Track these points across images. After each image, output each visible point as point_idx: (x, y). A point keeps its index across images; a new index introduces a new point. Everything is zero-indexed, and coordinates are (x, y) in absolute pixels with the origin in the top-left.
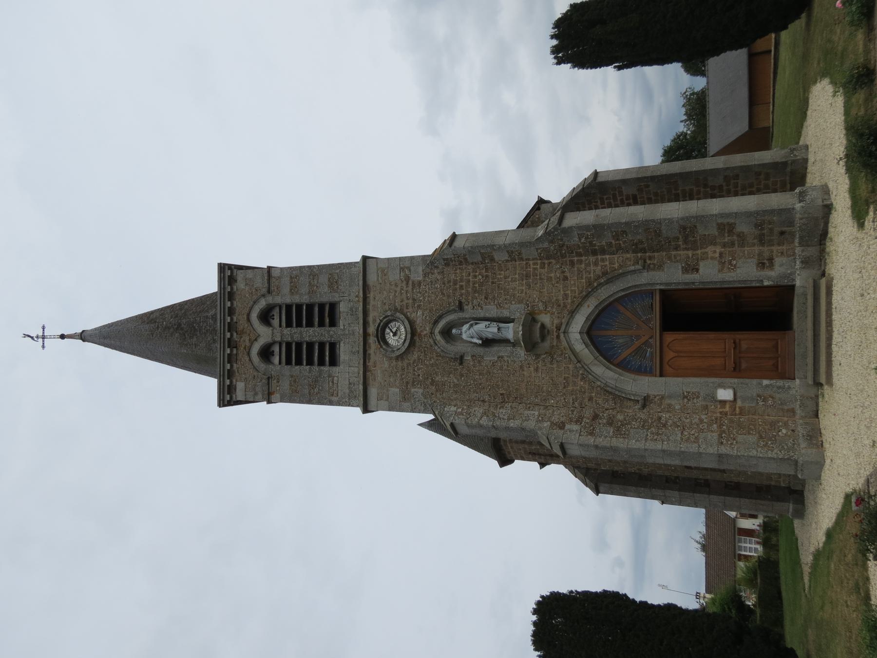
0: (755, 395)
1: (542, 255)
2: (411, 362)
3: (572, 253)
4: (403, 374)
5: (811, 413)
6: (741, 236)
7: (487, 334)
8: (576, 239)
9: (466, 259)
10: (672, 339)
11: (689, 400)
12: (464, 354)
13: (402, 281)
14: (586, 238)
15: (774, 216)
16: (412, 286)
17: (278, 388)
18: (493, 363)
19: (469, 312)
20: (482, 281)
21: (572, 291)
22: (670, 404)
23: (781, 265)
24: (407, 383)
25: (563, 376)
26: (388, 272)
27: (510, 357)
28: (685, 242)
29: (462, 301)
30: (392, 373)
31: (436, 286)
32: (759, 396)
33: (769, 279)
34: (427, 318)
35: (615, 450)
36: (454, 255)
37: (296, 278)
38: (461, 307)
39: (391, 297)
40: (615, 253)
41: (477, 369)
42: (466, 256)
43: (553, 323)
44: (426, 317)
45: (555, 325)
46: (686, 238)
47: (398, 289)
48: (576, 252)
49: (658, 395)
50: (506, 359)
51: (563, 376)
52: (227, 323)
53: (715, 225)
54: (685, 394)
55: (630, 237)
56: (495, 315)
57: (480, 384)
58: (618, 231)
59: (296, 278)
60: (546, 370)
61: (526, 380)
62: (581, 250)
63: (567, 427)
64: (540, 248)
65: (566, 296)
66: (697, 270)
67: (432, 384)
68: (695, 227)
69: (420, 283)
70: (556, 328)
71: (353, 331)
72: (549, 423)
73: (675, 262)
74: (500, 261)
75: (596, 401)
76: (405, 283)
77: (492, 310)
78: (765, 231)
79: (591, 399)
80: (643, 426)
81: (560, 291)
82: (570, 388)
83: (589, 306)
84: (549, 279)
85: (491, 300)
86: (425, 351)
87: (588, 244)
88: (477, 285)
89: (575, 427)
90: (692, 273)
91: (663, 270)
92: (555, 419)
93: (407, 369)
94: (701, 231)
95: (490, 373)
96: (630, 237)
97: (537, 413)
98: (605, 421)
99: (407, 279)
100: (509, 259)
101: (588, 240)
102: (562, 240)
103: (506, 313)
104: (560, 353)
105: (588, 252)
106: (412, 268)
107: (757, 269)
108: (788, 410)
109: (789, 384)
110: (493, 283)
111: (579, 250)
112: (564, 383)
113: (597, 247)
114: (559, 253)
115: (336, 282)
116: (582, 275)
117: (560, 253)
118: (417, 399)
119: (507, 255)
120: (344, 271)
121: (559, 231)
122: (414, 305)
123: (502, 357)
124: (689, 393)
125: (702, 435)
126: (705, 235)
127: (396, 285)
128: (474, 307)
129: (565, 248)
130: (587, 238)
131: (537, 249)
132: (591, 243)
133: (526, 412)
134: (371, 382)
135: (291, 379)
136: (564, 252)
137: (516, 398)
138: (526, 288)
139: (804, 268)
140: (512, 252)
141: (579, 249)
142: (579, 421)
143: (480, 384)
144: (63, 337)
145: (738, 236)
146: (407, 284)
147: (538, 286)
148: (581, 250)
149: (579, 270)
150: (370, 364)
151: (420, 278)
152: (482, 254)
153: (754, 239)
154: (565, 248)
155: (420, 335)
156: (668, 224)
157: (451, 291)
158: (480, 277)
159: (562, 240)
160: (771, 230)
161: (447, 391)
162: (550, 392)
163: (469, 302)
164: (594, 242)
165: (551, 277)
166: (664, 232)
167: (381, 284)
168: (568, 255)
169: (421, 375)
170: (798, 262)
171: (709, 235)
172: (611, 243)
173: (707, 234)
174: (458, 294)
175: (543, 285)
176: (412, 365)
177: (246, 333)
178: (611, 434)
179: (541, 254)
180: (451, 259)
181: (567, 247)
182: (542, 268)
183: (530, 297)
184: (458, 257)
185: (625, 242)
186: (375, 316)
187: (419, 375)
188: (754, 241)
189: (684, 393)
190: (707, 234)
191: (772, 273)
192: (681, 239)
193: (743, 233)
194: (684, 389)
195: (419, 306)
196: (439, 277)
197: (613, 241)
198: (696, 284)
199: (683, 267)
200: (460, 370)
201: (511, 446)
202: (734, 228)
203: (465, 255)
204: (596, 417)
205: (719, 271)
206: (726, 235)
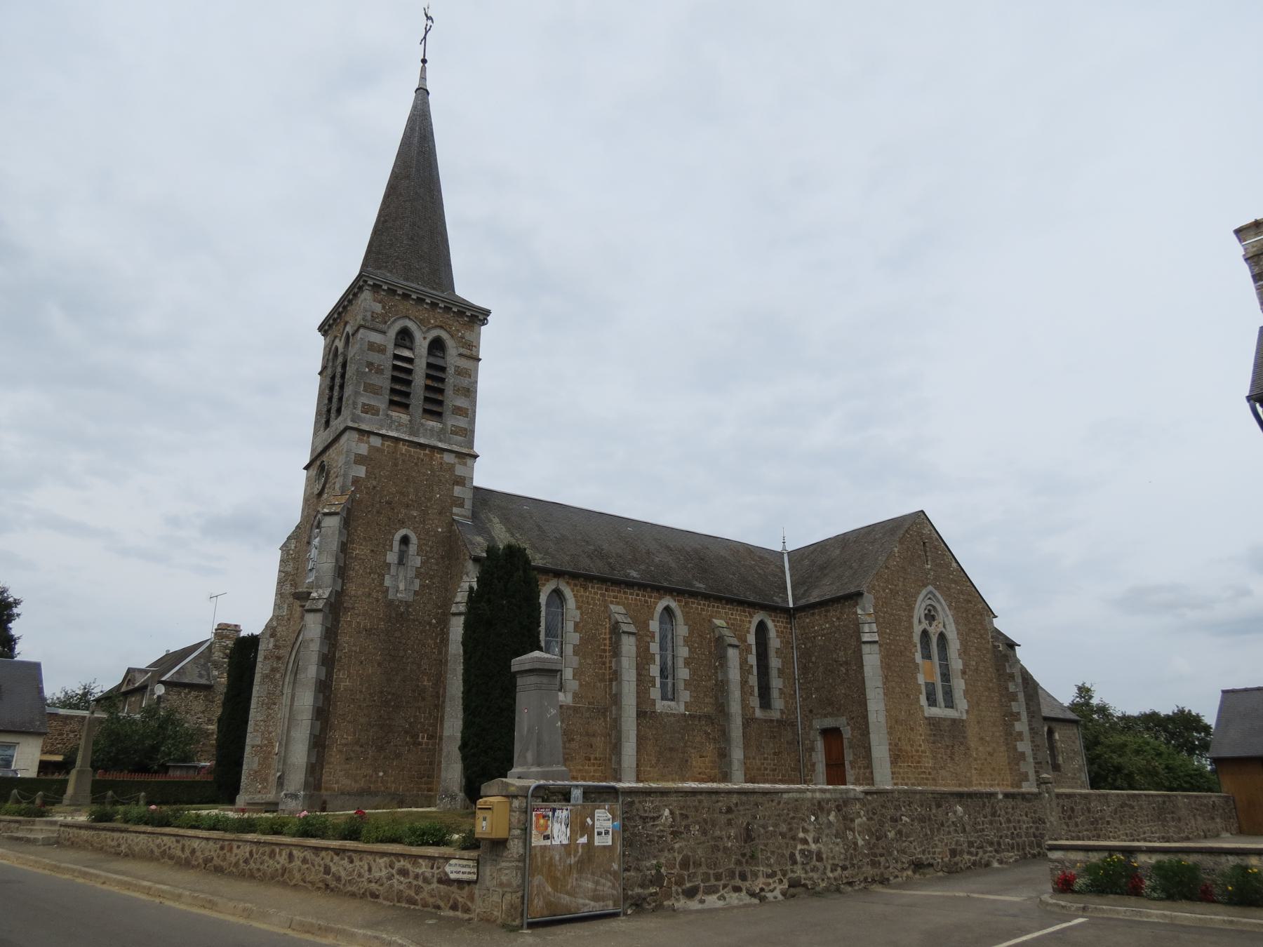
63: (272, 640)
72: (276, 625)
80: (270, 693)
89: (271, 646)
92: (280, 628)
97: (284, 614)
98: (275, 665)
125: (259, 734)
133: (286, 606)
142: (276, 647)
144: (424, 61)
178: (264, 672)
204: (279, 658)
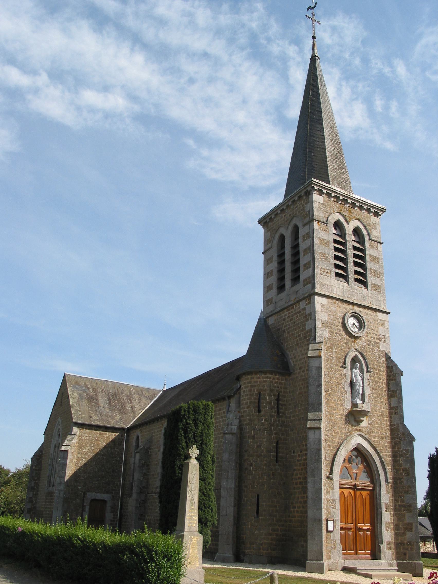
0: (336, 539)
1: (394, 426)
2: (341, 333)
3: (395, 444)
4: (335, 326)
5: (330, 567)
6: (404, 534)
7: (358, 385)
8: (405, 448)
9: (392, 380)
10: (352, 494)
11: (332, 503)
12: (347, 369)
13: (379, 336)
14: (406, 453)
15: (416, 551)
16: (377, 342)
17: (322, 229)
18: (343, 387)
19: (366, 376)
20: (380, 387)
21: (377, 441)
22: (330, 492)
23: (389, 553)
24: (331, 327)
25: (339, 431)
26: (383, 327)
27: (347, 399)
28: (400, 506)
29: (371, 373)
30: (336, 318)
31: (378, 358)
32: (336, 540)
33: (384, 547)
34: (363, 348)
35: (373, 467)
36: (395, 374)
37: (378, 262)
38: (368, 372)
39: (371, 326)
40: (394, 468)
41: (340, 377)
42: (395, 381)
43: (363, 428)
44: (363, 348)
45: (362, 429)
46: (404, 506)
47: (375, 332)
48: (395, 446)
49: (333, 486)
50: (345, 396)
51: (339, 431)
52: (379, 212)
53: (411, 521)
54: (335, 501)
55: (405, 477)
56: (365, 393)
57: (333, 377)
58: (409, 471)
59: (378, 262)
60: (341, 420)
61: (336, 407)
62: (397, 449)
64: (399, 426)
65: (375, 437)
66: (386, 511)
67: (331, 344)
68: (411, 512)
69: (378, 347)
70: (361, 429)
71: (354, 295)
73: (389, 499)
74: (390, 400)
75: (329, 449)
76: (378, 337)
77: (367, 392)
78: (406, 546)
79: (329, 446)
81: (377, 434)
82: (334, 434)
83: (371, 450)
84: (382, 429)
85: (372, 392)
86: (347, 343)
87: (401, 454)
88: (378, 384)
90: (385, 508)
91: (386, 493)
93: (338, 329)
94: (407, 514)
95: (338, 384)
96: (405, 477)
99: (380, 339)
100: (392, 406)
101: (404, 455)
102: (404, 440)
103: (366, 399)
104: (349, 430)
105: (395, 453)
106: (385, 344)
107: (387, 541)
108: (330, 556)
109: (341, 557)
110: (380, 394)
111: (396, 447)
112: (336, 431)
113: (398, 458)
114: (395, 436)
115: (376, 290)
116: (384, 448)
117: (395, 437)
118: (323, 332)
119: (394, 406)
120: (382, 297)
121: (411, 439)
122: (368, 341)
123: (346, 394)
124: (335, 503)
126: (405, 516)
127: (377, 331)
128: (368, 380)
129: (399, 440)
130: (405, 453)
131: (398, 425)
132: (402, 455)
134: (331, 301)
135: (327, 241)
136: (396, 439)
137: (327, 399)
138: (378, 414)
139: (389, 564)
140: (397, 410)
141: (397, 448)
143: (333, 377)
145: (403, 533)
146: (378, 339)
147: (379, 421)
148: (397, 449)
149: (386, 446)
150: (339, 303)
151: (381, 349)
152: (396, 391)
153: (401, 540)
154: (399, 440)
155: (355, 342)
156: (413, 498)
157: (375, 367)
158: (382, 387)
159: (404, 440)
160: (407, 549)
161: (328, 354)
162: (331, 422)
163: (371, 377)
164: (402, 457)
165: (383, 430)
166: (408, 495)
167: (377, 321)
168: (394, 441)
169: (335, 338)
170: (390, 561)
171: (405, 518)
172: (401, 466)
173: (406, 517)
174: (374, 371)
175: (379, 424)
176: (340, 332)
177: (349, 214)
179: (395, 426)
180: (393, 371)
181: (400, 442)
182: (386, 425)
183: (374, 415)
184: (394, 376)
185: (401, 474)
186: (363, 312)
187: (335, 336)
188: (400, 540)
189: (335, 500)
190: (406, 517)
191: (385, 549)
192: (402, 504)
193: (405, 535)
194: (336, 501)
195: (368, 344)
196: (381, 360)
197: (402, 468)
198: (380, 510)
199: (387, 503)
200: (339, 364)
201: (266, 381)
202: (409, 531)
203: (395, 380)
205: (386, 522)
206: (404, 527)
